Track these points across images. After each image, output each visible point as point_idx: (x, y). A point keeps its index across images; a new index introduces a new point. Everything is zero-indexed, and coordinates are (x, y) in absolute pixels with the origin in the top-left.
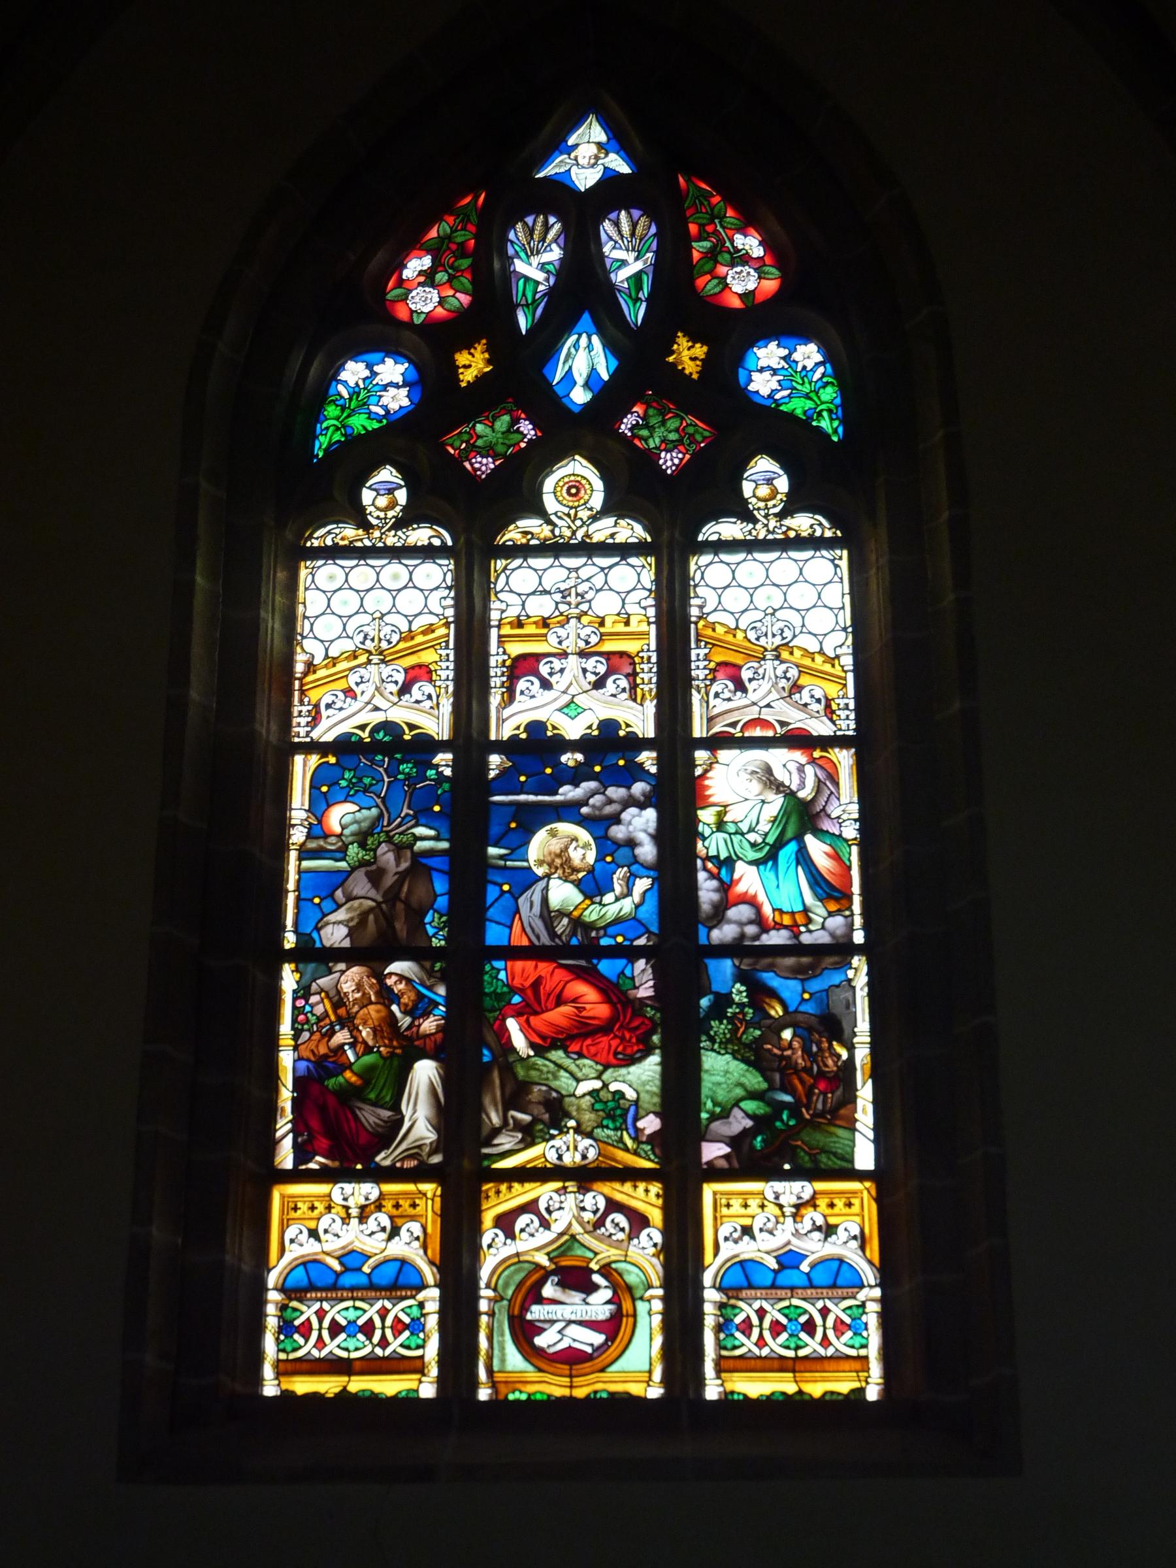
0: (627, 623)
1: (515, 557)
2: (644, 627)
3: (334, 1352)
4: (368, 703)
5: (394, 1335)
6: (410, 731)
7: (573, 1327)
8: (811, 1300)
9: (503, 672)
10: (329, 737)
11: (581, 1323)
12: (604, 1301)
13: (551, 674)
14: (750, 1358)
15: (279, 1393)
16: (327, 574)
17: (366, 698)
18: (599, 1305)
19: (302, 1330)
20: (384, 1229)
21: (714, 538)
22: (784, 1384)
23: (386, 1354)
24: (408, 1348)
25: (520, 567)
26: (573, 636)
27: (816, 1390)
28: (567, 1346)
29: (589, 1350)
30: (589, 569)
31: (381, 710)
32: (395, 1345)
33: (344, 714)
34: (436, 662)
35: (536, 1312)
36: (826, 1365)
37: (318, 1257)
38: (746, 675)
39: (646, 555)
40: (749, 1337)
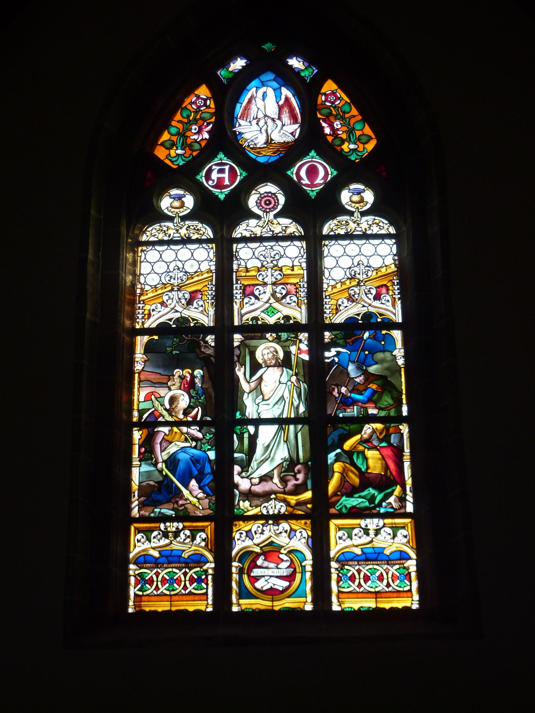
0: (293, 270)
1: (332, 240)
2: (301, 272)
3: (163, 591)
4: (173, 309)
5: (162, 585)
6: (193, 321)
7: (272, 578)
8: (180, 569)
9: (240, 292)
10: (154, 325)
11: (277, 577)
12: (286, 567)
13: (259, 294)
14: (151, 596)
15: (135, 611)
16: (152, 254)
17: (172, 306)
18: (284, 569)
19: (194, 581)
20: (189, 537)
21: (239, 236)
22: (370, 604)
23: (186, 593)
24: (197, 589)
25: (334, 244)
26: (270, 275)
27: (386, 605)
28: (270, 587)
29: (281, 589)
30: (278, 247)
31: (178, 312)
32: (190, 588)
33: (160, 314)
34: (207, 291)
35: (256, 572)
36: (402, 595)
37: (251, 549)
38: (257, 293)
39: (211, 243)
40: (354, 583)
